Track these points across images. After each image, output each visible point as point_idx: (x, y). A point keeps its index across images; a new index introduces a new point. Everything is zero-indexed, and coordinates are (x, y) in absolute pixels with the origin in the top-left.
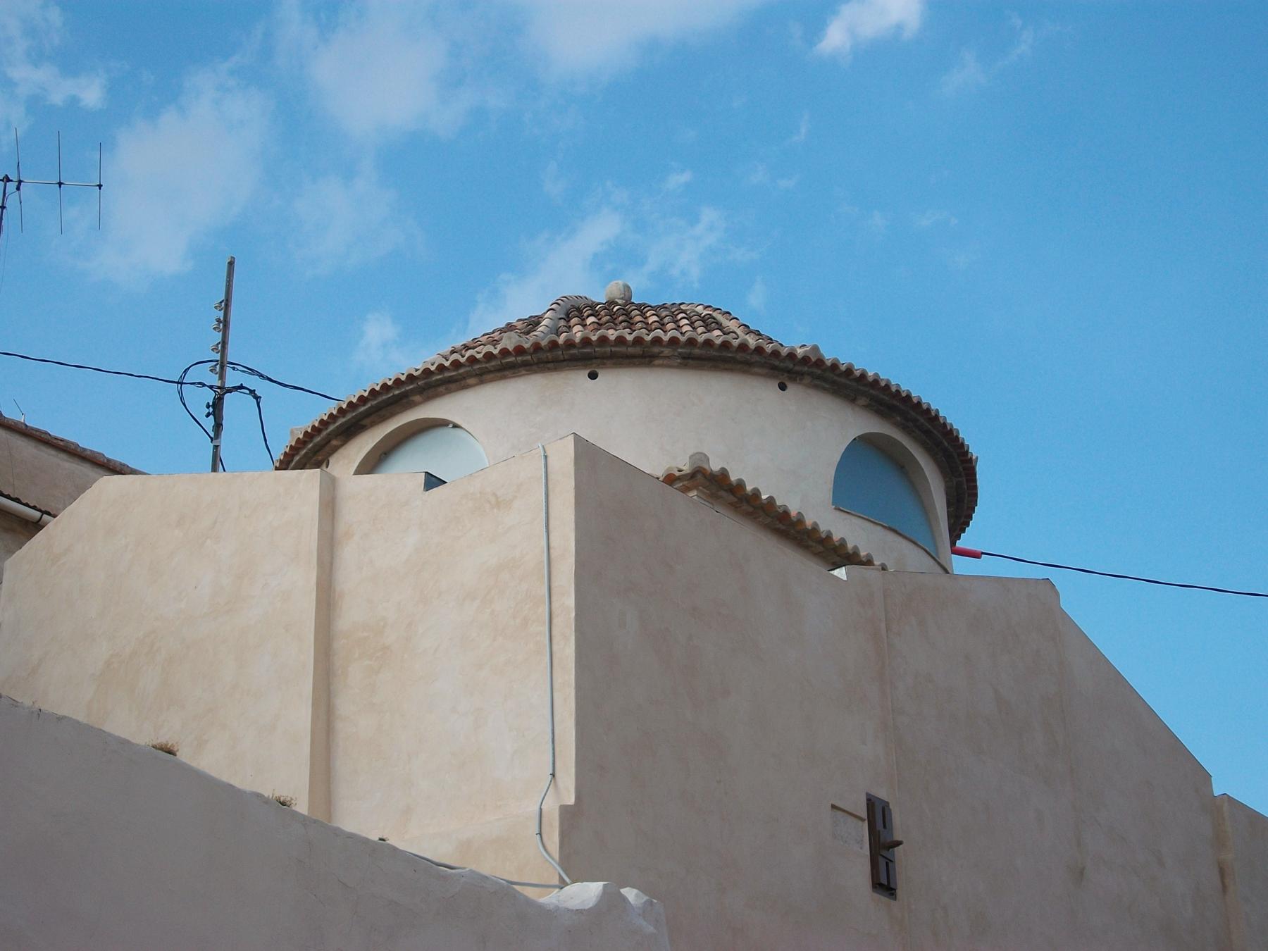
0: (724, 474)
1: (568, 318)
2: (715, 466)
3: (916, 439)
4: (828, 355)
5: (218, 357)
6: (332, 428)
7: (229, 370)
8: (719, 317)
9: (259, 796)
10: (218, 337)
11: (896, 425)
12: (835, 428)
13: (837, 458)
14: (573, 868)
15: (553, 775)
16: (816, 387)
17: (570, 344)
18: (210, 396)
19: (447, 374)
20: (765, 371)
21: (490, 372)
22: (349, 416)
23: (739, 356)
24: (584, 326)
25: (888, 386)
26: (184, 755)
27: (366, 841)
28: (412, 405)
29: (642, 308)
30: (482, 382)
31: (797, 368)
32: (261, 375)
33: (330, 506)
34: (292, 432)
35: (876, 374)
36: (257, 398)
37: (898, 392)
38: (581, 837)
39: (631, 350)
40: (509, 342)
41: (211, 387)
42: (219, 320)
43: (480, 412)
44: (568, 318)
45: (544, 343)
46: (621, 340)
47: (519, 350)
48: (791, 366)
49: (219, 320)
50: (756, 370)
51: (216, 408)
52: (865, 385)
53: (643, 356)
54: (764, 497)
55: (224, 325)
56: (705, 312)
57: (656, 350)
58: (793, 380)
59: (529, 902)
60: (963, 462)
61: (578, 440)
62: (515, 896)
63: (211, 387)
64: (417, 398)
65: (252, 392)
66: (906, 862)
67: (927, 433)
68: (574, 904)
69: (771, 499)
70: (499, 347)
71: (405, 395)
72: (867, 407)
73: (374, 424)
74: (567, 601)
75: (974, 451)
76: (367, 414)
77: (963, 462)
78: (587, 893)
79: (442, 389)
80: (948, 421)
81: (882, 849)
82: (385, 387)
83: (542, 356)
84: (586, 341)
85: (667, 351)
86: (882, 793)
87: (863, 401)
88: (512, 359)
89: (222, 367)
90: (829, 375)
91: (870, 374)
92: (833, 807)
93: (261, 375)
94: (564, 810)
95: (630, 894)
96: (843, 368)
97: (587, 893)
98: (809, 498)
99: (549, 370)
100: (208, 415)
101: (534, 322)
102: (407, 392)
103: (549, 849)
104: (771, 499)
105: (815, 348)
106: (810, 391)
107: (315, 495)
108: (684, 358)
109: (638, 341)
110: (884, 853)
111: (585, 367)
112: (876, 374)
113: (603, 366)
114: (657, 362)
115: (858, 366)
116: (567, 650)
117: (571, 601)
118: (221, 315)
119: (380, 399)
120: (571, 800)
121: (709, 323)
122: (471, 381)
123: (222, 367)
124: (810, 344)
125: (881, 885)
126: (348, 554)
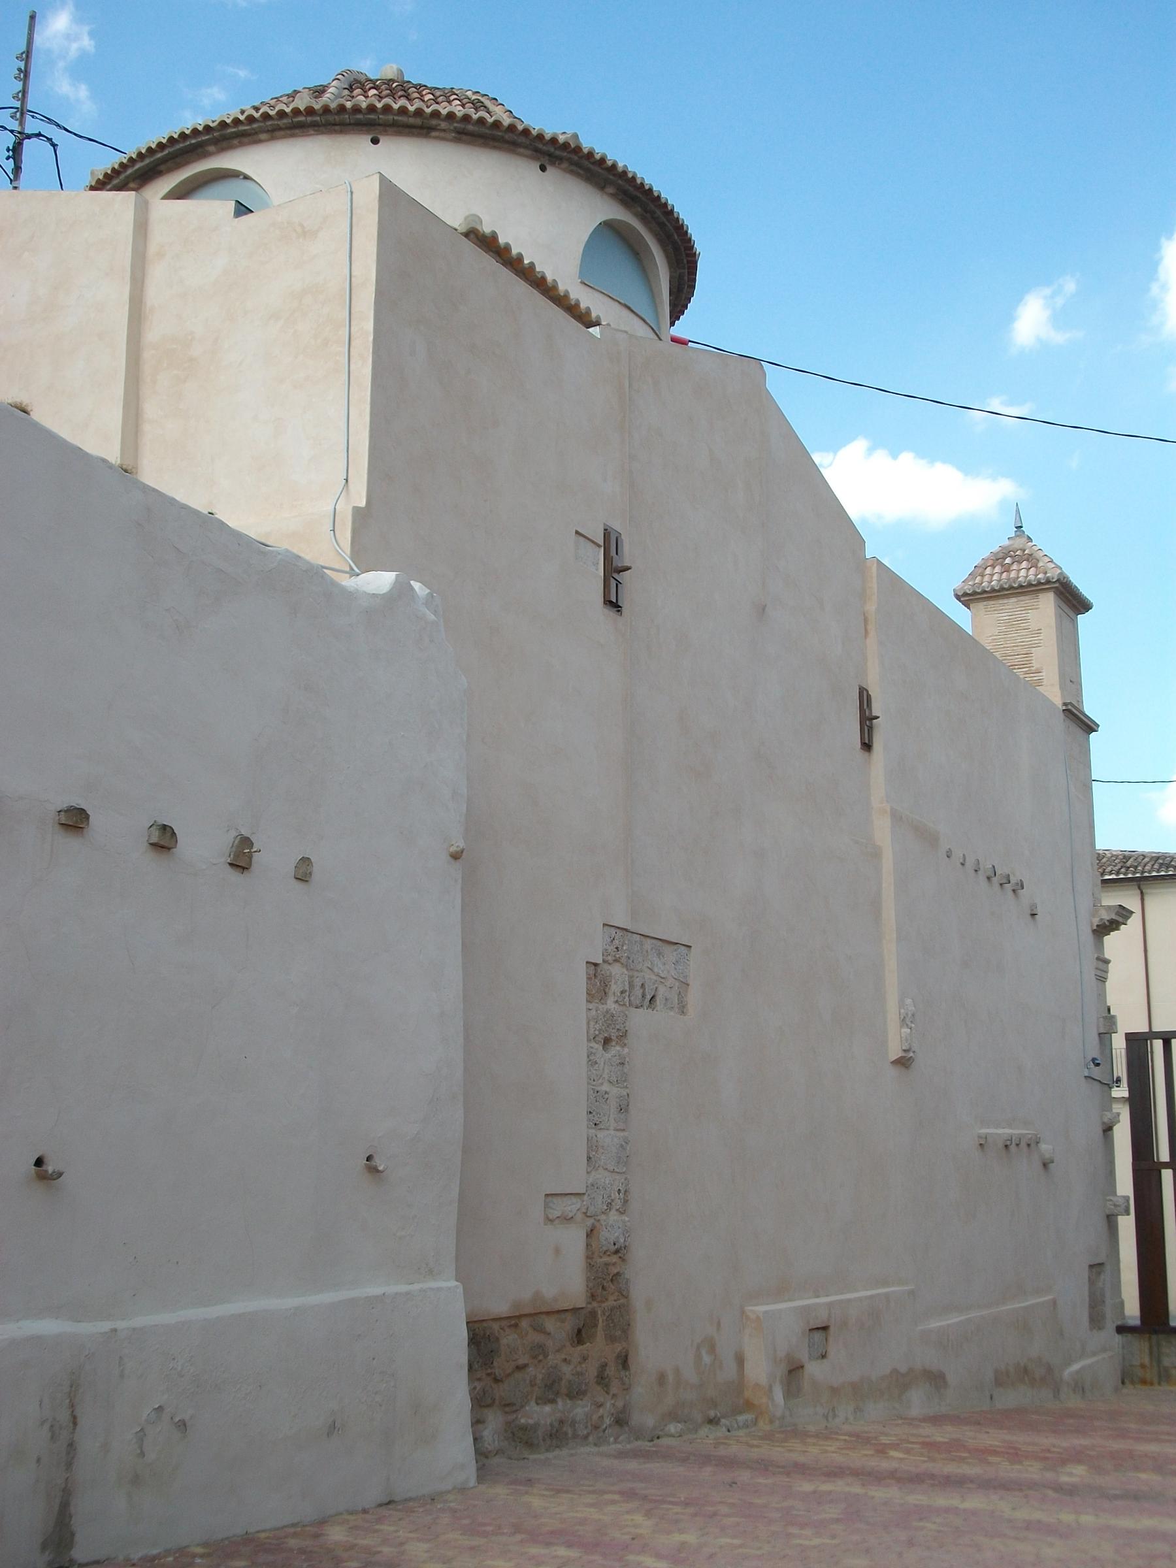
0: (494, 237)
1: (351, 88)
2: (487, 229)
3: (651, 230)
4: (586, 144)
5: (18, 104)
6: (130, 171)
7: (28, 117)
8: (487, 103)
9: (104, 461)
10: (19, 86)
11: (636, 215)
12: (588, 210)
13: (586, 237)
14: (364, 556)
15: (347, 480)
16: (572, 172)
17: (356, 109)
18: (10, 140)
19: (242, 128)
20: (529, 152)
21: (280, 129)
22: (147, 161)
23: (508, 136)
24: (367, 97)
25: (634, 178)
26: (36, 416)
27: (196, 513)
28: (206, 155)
29: (419, 87)
30: (273, 138)
31: (558, 153)
32: (58, 125)
33: (142, 227)
34: (92, 173)
35: (625, 166)
36: (54, 145)
37: (642, 184)
38: (370, 534)
39: (412, 121)
40: (301, 103)
41: (12, 131)
42: (20, 70)
43: (269, 166)
44: (351, 88)
45: (333, 106)
46: (403, 111)
47: (310, 111)
48: (552, 150)
49: (20, 70)
50: (521, 150)
51: (16, 152)
52: (614, 175)
53: (421, 127)
54: (526, 262)
55: (24, 75)
56: (474, 97)
57: (434, 122)
58: (553, 164)
59: (334, 583)
60: (687, 255)
61: (383, 180)
62: (323, 576)
63: (12, 131)
64: (211, 148)
65: (49, 140)
66: (632, 587)
67: (662, 225)
68: (371, 589)
69: (532, 265)
70: (292, 106)
71: (201, 145)
72: (613, 196)
73: (170, 170)
74: (366, 325)
75: (698, 247)
76: (164, 161)
77: (687, 255)
78: (381, 581)
79: (235, 142)
80: (681, 217)
81: (613, 571)
82: (183, 136)
83: (330, 118)
84: (372, 109)
85: (443, 125)
86: (616, 525)
87: (611, 190)
88: (302, 119)
89: (22, 114)
90: (586, 163)
91: (620, 165)
92: (577, 533)
93: (58, 125)
94: (356, 510)
95: (416, 585)
96: (598, 157)
97: (381, 581)
98: (561, 266)
99: (336, 132)
100: (8, 158)
101: (319, 91)
102: (203, 142)
103: (342, 544)
104: (532, 265)
105: (575, 136)
106: (568, 176)
107: (129, 215)
108: (459, 133)
109: (419, 112)
110: (615, 576)
111: (368, 132)
112: (625, 166)
113: (385, 133)
114: (434, 134)
115: (611, 157)
116: (364, 370)
117: (370, 326)
118: (22, 65)
119: (178, 147)
120: (362, 503)
121: (477, 105)
122: (263, 136)
123: (22, 114)
124: (570, 132)
125: (611, 602)
126: (157, 274)
